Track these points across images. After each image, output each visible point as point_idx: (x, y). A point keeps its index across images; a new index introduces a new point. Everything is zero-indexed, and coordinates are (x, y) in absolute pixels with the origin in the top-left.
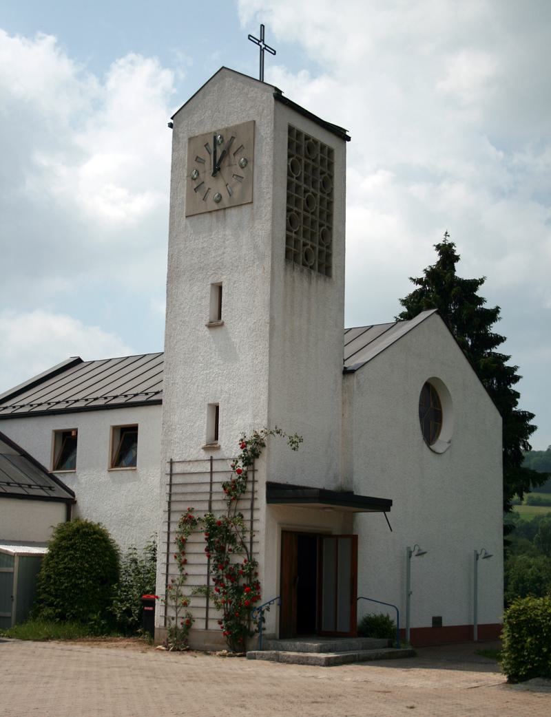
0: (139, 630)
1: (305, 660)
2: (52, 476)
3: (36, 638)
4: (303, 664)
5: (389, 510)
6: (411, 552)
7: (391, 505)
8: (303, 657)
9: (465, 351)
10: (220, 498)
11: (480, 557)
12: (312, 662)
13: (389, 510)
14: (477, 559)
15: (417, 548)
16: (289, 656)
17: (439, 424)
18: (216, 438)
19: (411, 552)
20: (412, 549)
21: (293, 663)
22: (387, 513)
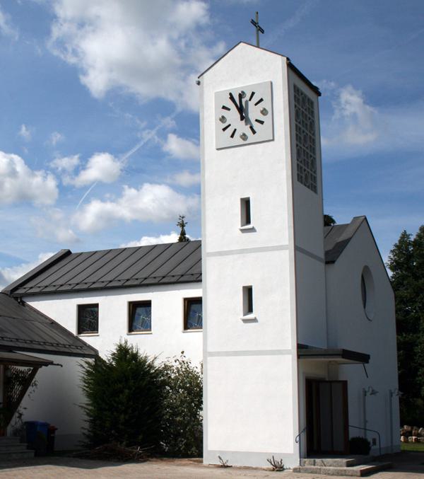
0: (24, 131)
1: (343, 472)
2: (77, 339)
3: (43, 318)
4: (342, 475)
5: (368, 362)
6: (366, 392)
7: (369, 358)
8: (341, 471)
9: (48, 321)
10: (37, 323)
11: (368, 394)
12: (350, 474)
13: (368, 362)
14: (365, 395)
15: (371, 389)
16: (329, 470)
17: (400, 317)
18: (250, 100)
19: (366, 392)
20: (367, 390)
21: (333, 475)
22: (366, 365)
